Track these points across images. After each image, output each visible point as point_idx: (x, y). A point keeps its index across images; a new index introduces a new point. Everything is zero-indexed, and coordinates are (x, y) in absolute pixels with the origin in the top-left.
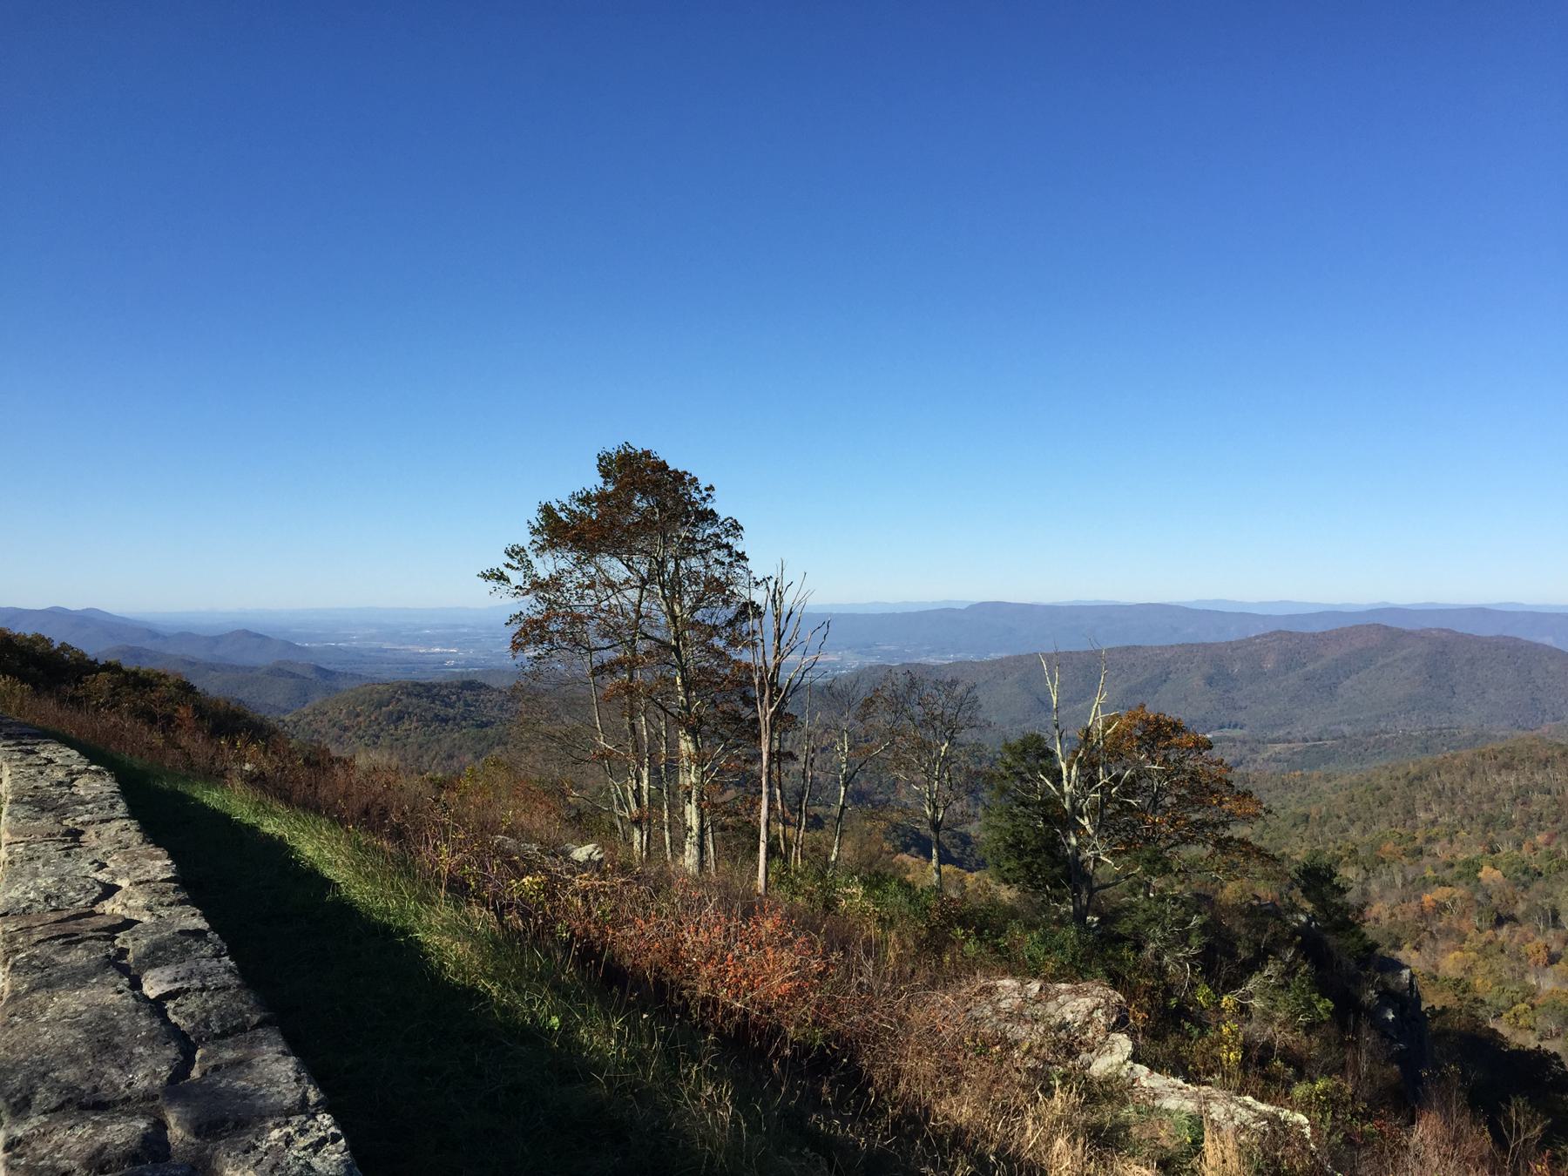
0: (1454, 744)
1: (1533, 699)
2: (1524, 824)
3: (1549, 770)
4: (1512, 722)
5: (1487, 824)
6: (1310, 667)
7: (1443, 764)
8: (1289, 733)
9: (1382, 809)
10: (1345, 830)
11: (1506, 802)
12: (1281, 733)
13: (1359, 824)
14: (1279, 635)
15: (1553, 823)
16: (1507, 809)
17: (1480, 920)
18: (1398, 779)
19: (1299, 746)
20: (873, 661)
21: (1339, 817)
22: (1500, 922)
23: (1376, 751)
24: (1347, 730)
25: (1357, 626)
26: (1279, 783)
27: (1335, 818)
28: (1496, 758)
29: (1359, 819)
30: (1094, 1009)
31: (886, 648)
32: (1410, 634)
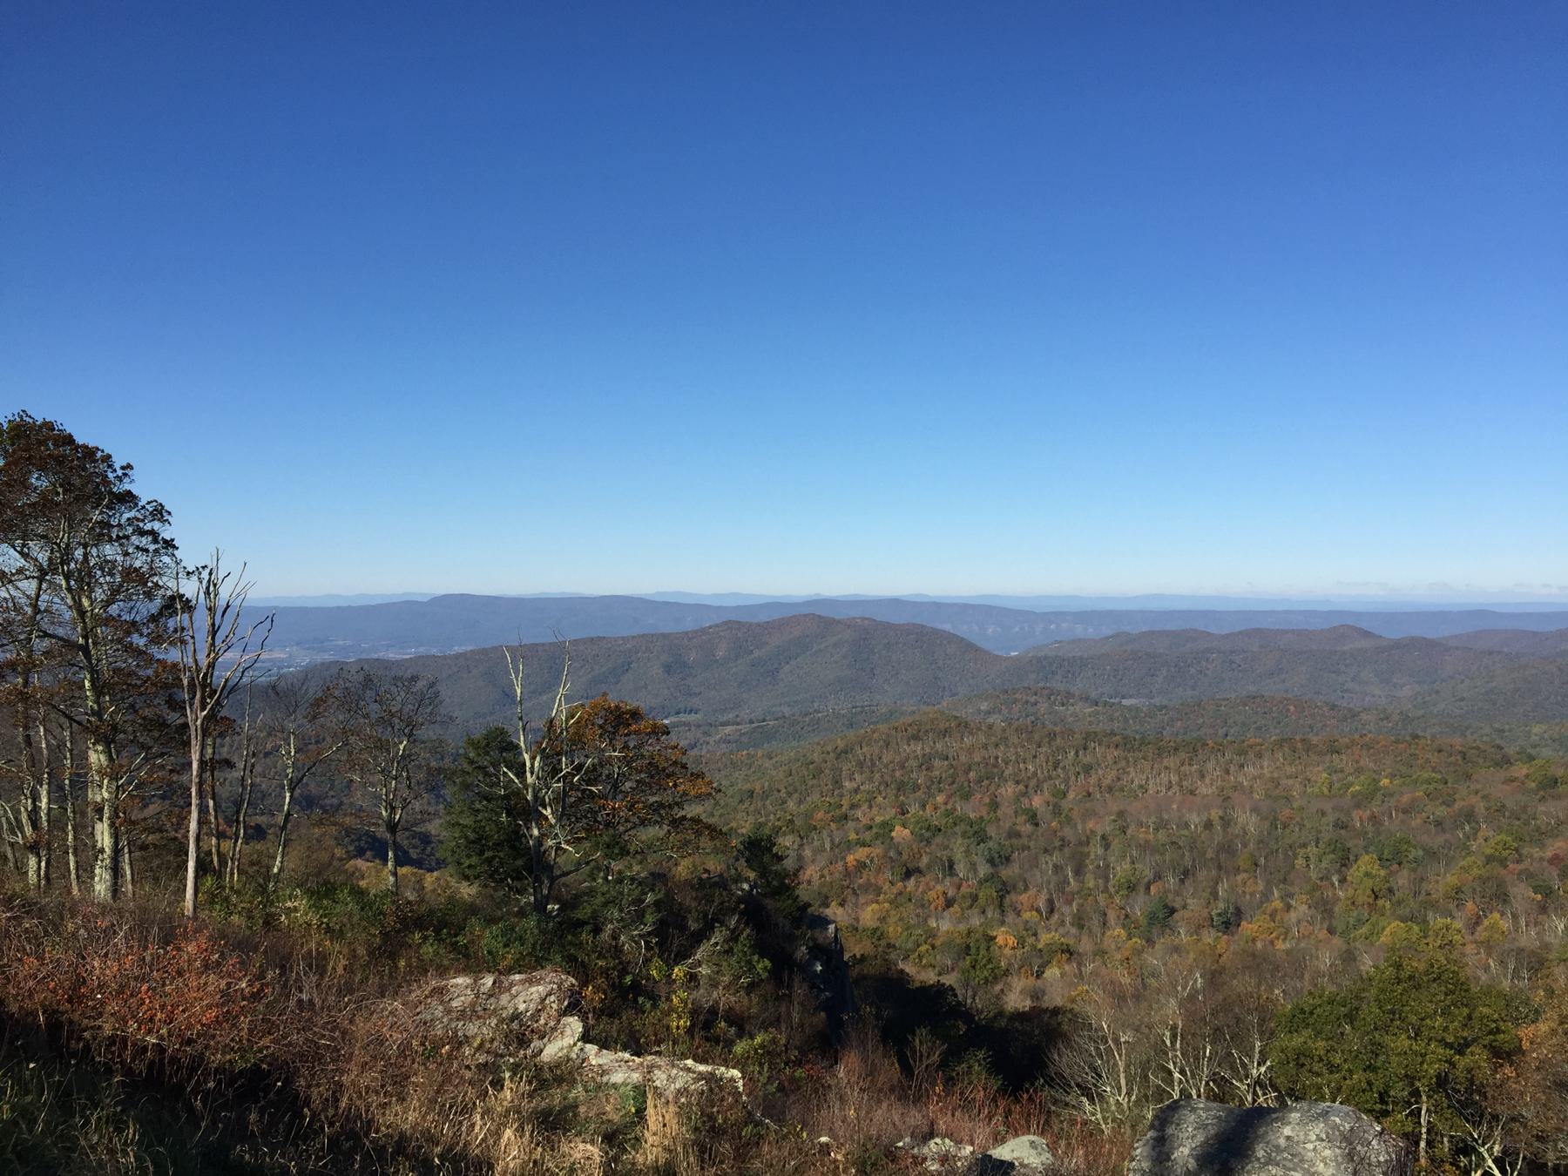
0: (874, 720)
3: (947, 739)
6: (756, 654)
8: (737, 716)
9: (815, 781)
10: (784, 802)
12: (731, 716)
13: (796, 795)
14: (729, 625)
16: (914, 775)
17: (893, 874)
18: (828, 753)
19: (745, 728)
20: (327, 657)
21: (779, 791)
23: (810, 729)
24: (787, 711)
25: (795, 616)
26: (729, 763)
27: (775, 793)
28: (906, 731)
29: (796, 791)
31: (341, 643)
32: (839, 622)
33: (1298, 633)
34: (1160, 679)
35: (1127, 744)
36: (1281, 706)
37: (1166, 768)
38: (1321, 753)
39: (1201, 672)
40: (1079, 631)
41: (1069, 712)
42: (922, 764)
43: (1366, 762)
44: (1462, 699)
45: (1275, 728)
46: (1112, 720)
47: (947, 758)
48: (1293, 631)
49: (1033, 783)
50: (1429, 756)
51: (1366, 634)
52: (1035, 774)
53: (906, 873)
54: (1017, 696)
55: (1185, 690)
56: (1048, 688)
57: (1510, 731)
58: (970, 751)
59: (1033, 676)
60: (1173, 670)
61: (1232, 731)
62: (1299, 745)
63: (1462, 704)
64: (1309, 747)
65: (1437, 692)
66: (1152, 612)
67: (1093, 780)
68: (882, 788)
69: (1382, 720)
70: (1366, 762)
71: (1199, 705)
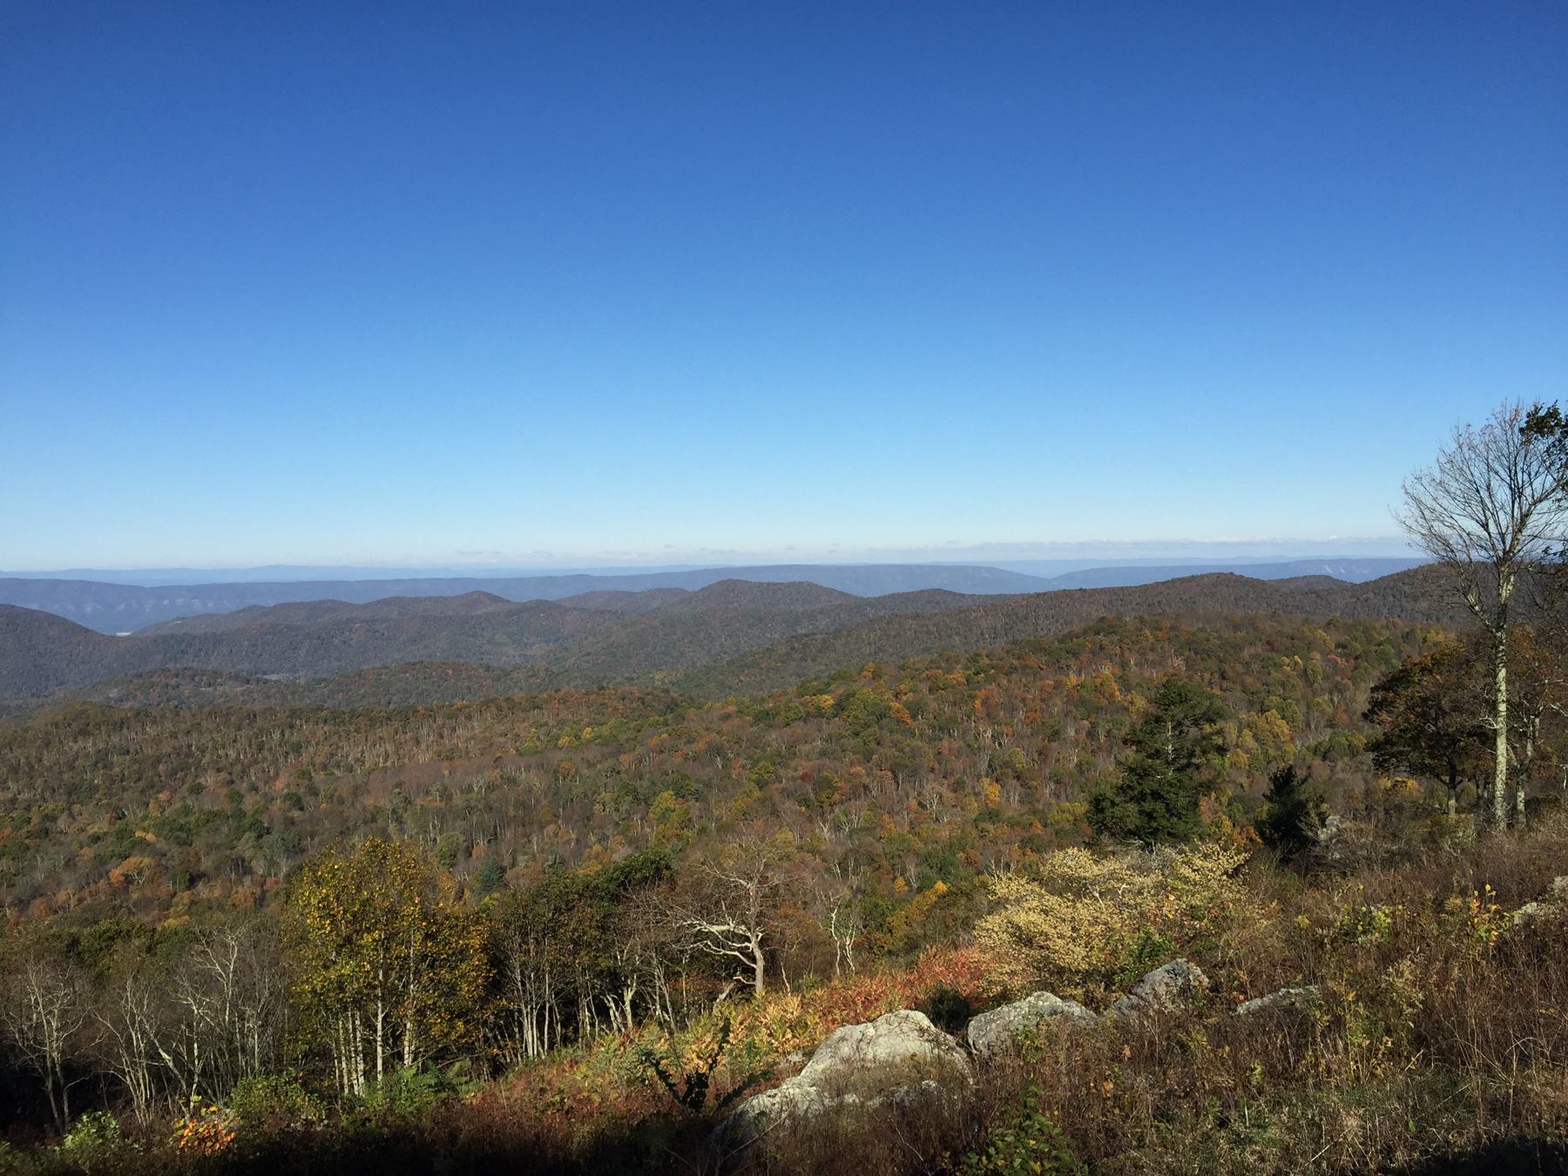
1: (36, 666)
2: (107, 788)
3: (125, 731)
4: (15, 691)
5: (70, 794)
7: (15, 739)
11: (88, 769)
15: (135, 782)
16: (89, 776)
17: (174, 883)
22: (192, 881)
30: (746, 1085)
33: (437, 600)
34: (303, 652)
35: (336, 717)
36: (440, 670)
37: (381, 738)
38: (525, 710)
39: (345, 642)
40: (198, 606)
41: (217, 693)
42: (97, 762)
43: (564, 714)
44: (588, 654)
45: (436, 691)
46: (268, 697)
47: (128, 752)
48: (429, 599)
49: (238, 768)
50: (615, 703)
51: (496, 599)
52: (238, 759)
53: (189, 880)
54: (154, 679)
55: (330, 662)
56: (190, 669)
57: (638, 678)
58: (157, 741)
59: (159, 657)
60: (315, 641)
61: (395, 699)
62: (504, 704)
63: (589, 658)
64: (512, 705)
65: (566, 649)
66: (397, 581)
67: (305, 758)
68: (47, 795)
69: (531, 676)
70: (564, 714)
71: (360, 676)
